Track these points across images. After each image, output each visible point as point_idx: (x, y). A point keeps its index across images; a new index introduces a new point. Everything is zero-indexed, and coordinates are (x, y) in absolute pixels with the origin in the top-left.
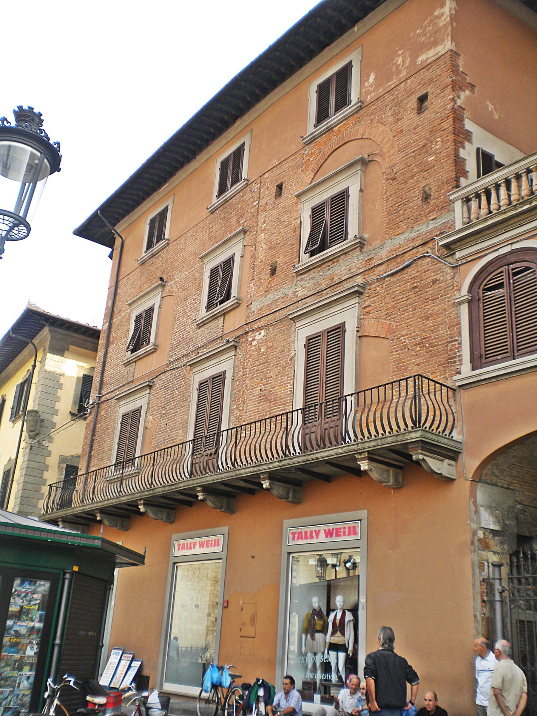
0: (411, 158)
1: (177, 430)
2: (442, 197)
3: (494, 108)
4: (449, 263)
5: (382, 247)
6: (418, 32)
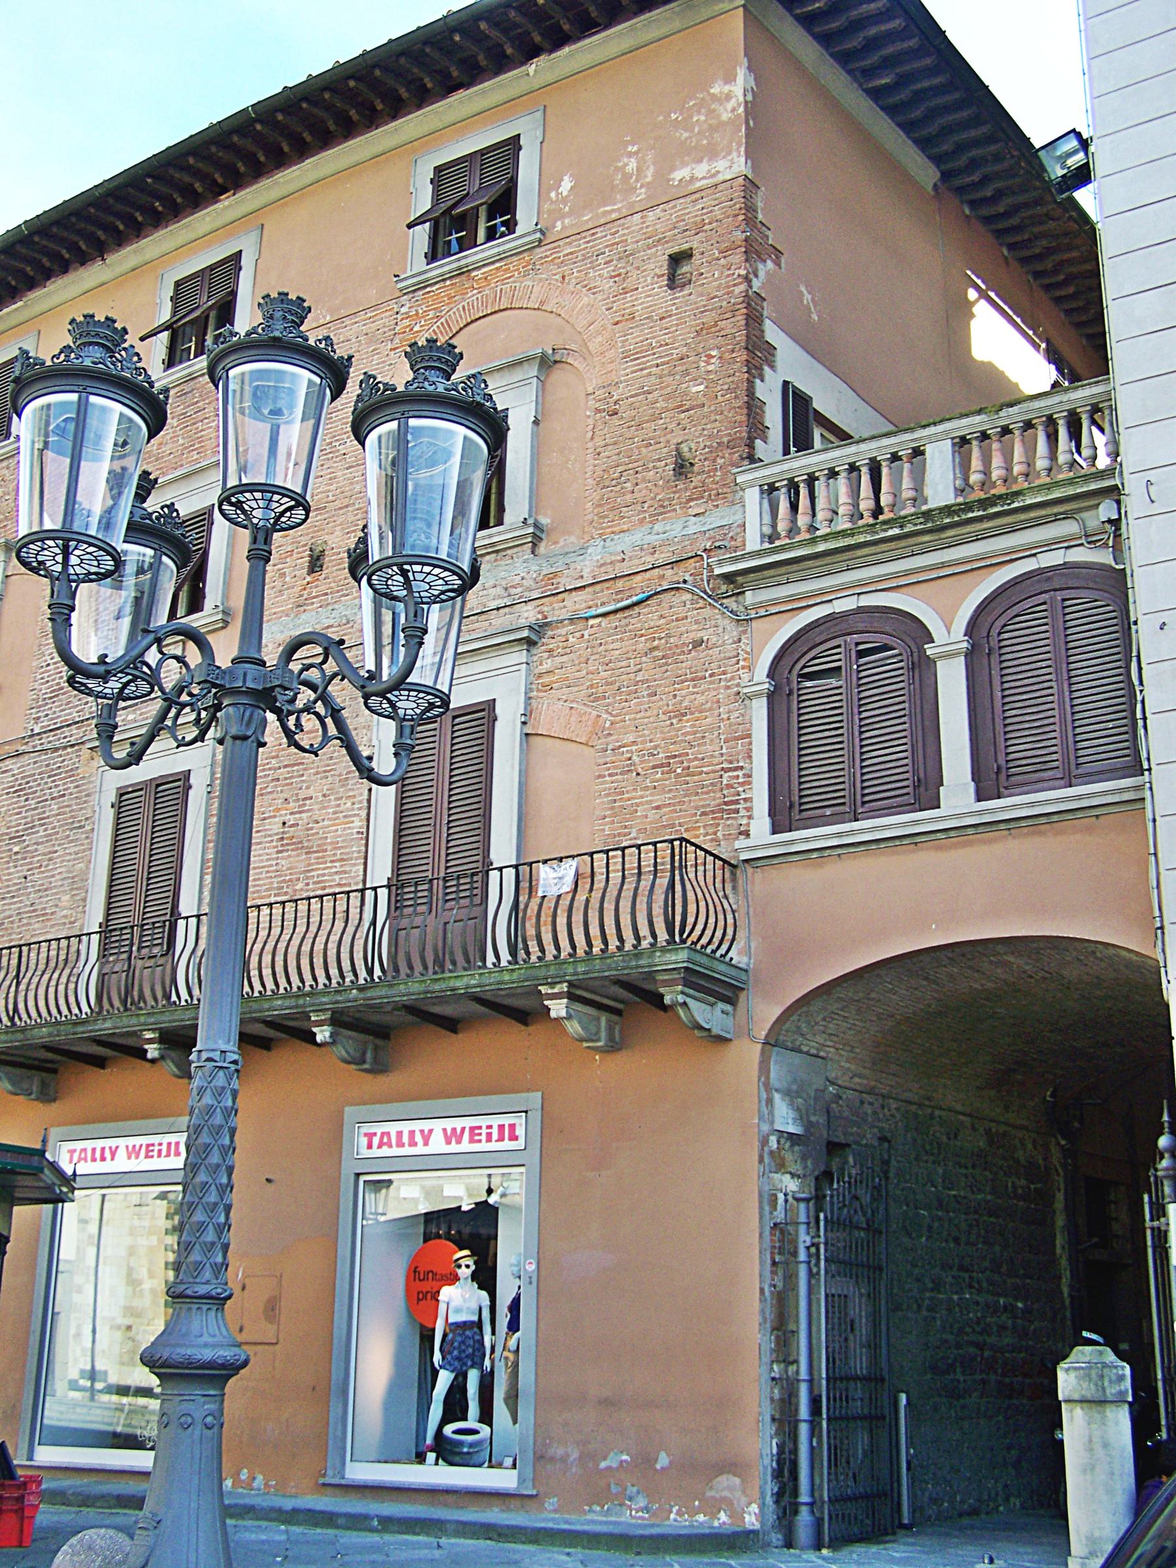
0: (653, 378)
1: (56, 894)
2: (719, 473)
3: (813, 300)
4: (731, 612)
5: (582, 551)
6: (673, 116)
